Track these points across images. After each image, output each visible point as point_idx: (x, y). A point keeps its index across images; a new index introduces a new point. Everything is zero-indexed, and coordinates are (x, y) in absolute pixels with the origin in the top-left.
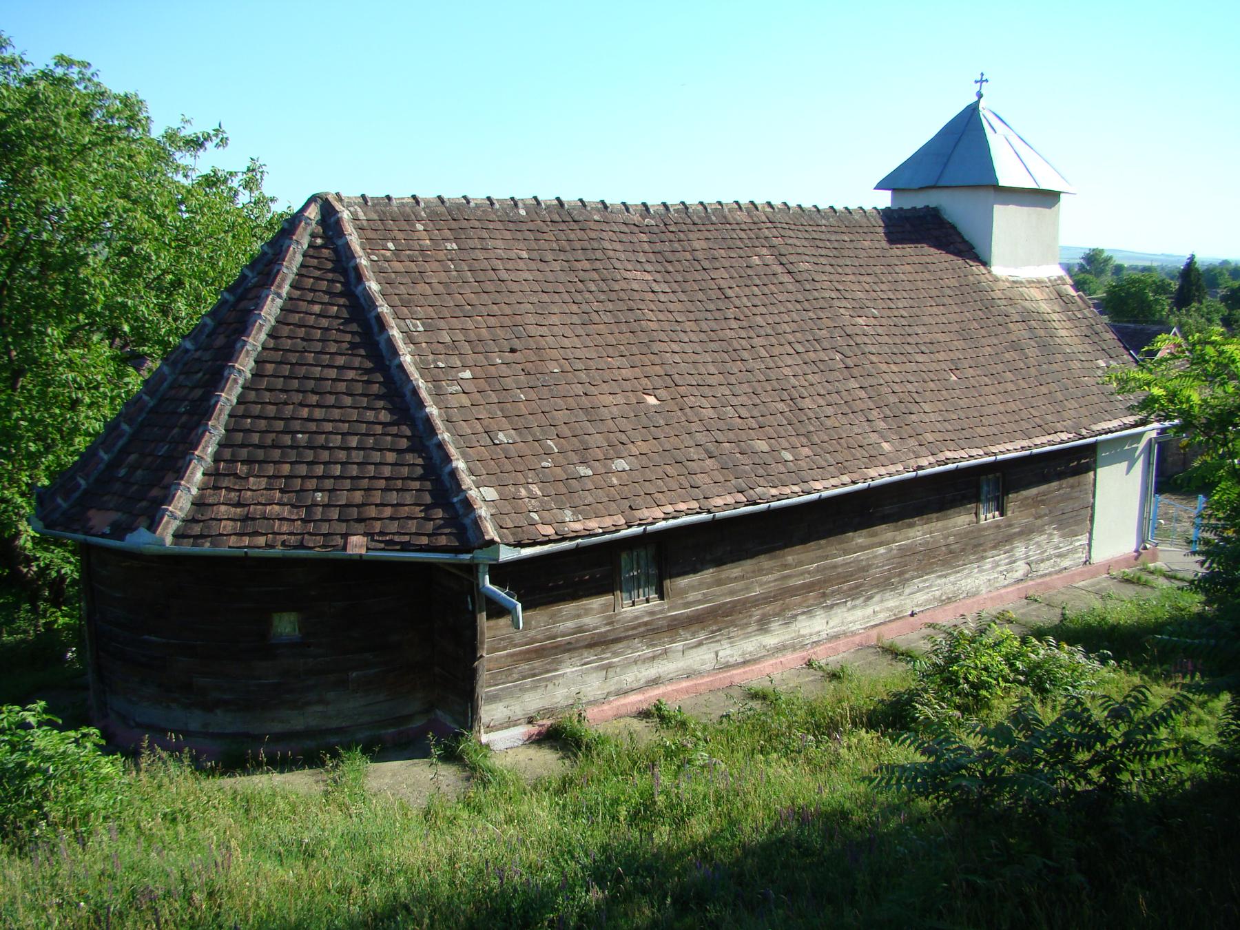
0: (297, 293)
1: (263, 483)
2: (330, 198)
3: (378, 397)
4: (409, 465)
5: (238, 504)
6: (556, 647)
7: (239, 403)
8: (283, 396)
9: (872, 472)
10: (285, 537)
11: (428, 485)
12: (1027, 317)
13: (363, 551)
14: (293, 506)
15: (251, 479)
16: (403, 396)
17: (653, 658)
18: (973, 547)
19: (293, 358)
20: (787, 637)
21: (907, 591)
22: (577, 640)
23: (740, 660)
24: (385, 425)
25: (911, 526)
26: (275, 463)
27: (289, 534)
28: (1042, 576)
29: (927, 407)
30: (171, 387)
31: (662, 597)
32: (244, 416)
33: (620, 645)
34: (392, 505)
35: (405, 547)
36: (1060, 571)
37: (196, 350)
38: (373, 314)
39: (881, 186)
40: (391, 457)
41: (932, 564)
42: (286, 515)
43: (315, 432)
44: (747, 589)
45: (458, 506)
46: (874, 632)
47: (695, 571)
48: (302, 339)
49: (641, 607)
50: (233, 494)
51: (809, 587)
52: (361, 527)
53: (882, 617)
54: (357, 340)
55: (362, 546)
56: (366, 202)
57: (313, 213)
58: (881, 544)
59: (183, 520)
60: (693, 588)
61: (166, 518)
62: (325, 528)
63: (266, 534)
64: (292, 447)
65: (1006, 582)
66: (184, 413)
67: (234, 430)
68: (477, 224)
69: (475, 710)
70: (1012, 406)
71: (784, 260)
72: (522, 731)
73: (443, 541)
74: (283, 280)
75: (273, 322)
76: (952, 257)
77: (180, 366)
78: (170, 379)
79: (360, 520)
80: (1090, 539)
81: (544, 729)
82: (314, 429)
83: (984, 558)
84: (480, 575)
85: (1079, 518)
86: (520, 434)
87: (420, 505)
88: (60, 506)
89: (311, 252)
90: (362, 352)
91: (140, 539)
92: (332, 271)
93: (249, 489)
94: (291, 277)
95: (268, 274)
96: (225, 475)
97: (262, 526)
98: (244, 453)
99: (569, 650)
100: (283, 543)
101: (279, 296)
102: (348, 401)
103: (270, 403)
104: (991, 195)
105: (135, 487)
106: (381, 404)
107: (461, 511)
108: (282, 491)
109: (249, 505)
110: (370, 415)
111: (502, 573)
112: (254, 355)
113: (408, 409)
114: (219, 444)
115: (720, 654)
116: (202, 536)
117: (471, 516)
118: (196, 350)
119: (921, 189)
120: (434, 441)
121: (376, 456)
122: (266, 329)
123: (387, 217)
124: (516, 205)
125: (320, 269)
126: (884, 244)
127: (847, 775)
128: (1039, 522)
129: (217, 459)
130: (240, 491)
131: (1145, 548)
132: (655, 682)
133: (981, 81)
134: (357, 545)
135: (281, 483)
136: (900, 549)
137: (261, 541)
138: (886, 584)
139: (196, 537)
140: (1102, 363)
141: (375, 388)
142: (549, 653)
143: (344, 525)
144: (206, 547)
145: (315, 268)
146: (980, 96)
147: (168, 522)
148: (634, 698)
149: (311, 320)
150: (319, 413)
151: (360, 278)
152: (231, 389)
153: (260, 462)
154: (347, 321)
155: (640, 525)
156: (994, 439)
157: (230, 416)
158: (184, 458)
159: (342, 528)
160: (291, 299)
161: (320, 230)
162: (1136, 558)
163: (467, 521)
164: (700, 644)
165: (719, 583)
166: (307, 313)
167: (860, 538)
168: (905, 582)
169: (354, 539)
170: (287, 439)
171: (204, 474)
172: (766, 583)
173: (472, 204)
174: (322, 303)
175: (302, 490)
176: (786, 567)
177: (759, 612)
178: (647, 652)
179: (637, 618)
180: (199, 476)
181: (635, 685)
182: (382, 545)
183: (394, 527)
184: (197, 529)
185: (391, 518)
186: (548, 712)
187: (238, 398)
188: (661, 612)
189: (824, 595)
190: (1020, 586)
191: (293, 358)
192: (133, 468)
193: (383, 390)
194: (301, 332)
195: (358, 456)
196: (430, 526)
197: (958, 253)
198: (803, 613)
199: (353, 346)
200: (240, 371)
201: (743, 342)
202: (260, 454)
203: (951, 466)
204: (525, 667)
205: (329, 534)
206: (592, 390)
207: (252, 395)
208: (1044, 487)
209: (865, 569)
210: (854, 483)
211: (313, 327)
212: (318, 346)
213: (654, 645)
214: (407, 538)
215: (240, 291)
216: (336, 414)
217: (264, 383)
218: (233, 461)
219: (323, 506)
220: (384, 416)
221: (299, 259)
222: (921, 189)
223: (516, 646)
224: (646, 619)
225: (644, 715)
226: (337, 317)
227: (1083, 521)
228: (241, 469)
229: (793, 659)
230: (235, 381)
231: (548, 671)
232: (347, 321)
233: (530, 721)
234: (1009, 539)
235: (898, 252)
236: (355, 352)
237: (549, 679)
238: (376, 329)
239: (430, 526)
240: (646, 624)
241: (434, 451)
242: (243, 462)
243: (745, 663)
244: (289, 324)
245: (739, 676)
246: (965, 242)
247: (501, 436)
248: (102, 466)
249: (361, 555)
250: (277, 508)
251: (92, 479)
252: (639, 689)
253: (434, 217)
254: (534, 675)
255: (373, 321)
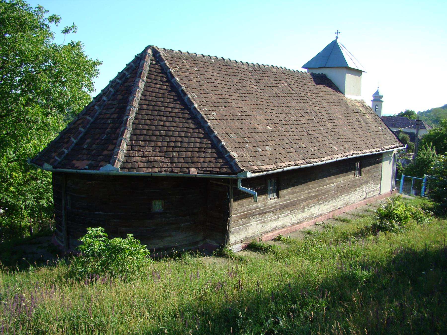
0: (149, 80)
1: (151, 149)
2: (155, 47)
3: (188, 119)
4: (205, 143)
5: (144, 156)
6: (250, 214)
7: (135, 119)
8: (152, 117)
9: (336, 156)
10: (165, 169)
11: (214, 150)
12: (358, 111)
13: (197, 174)
14: (165, 157)
15: (146, 147)
16: (198, 119)
17: (275, 220)
18: (353, 186)
19: (153, 103)
20: (309, 214)
21: (338, 200)
22: (256, 212)
23: (297, 222)
24: (193, 129)
25: (339, 177)
26: (154, 141)
27: (166, 167)
28: (369, 198)
29: (342, 137)
30: (100, 114)
31: (278, 198)
32: (139, 124)
33: (267, 214)
34: (203, 157)
35: (211, 172)
36: (373, 197)
37: (108, 101)
38: (180, 89)
39: (304, 67)
40: (198, 140)
41: (344, 191)
42: (163, 160)
43: (168, 131)
44: (300, 196)
45: (227, 158)
46: (331, 214)
47: (287, 188)
48: (155, 97)
49: (273, 201)
50: (140, 153)
51: (315, 196)
52: (193, 165)
53: (332, 209)
54: (176, 98)
55: (195, 172)
56: (166, 51)
57: (150, 51)
58: (332, 183)
59: (123, 162)
60: (287, 195)
61: (117, 161)
62: (180, 165)
63: (157, 168)
64: (160, 136)
65: (361, 199)
66: (111, 123)
67: (136, 129)
68: (201, 63)
69: (228, 237)
70: (363, 139)
71: (290, 86)
72: (240, 246)
73: (225, 170)
74: (144, 75)
75: (143, 90)
76: (333, 90)
77: (102, 106)
78: (99, 111)
79: (193, 162)
80: (380, 186)
81: (246, 245)
82: (167, 129)
83: (356, 190)
84: (239, 183)
85: (378, 179)
86: (236, 135)
87: (213, 157)
88: (57, 160)
89: (152, 66)
90: (179, 103)
91: (106, 169)
92: (160, 73)
93: (146, 151)
94: (146, 75)
95: (136, 73)
96: (136, 146)
97: (155, 165)
98: (141, 137)
99: (253, 215)
100: (165, 171)
101: (143, 81)
102: (177, 120)
103: (148, 119)
104: (345, 70)
105: (94, 151)
106: (190, 121)
107: (229, 160)
108: (159, 152)
109: (148, 157)
110: (187, 125)
111: (248, 182)
112: (138, 101)
113: (201, 124)
114: (131, 134)
115: (293, 219)
116: (132, 168)
117: (234, 161)
118: (108, 101)
119: (319, 68)
120: (213, 135)
121: (193, 140)
122: (141, 92)
123: (177, 57)
124: (211, 58)
125: (156, 72)
126: (314, 84)
127: (319, 268)
128: (369, 179)
129: (131, 140)
130: (143, 151)
131: (393, 190)
132: (275, 229)
133: (338, 33)
134: (194, 172)
135: (158, 149)
136: (337, 185)
137: (156, 170)
138: (334, 197)
139: (129, 168)
140: (380, 128)
141: (187, 116)
142: (248, 216)
143: (187, 164)
144: (134, 172)
145: (155, 72)
146: (337, 38)
147: (117, 163)
148: (270, 234)
149: (157, 90)
150: (167, 124)
151: (172, 77)
152: (132, 114)
153: (148, 141)
154: (170, 91)
155: (280, 168)
156: (361, 148)
157: (133, 124)
158: (117, 139)
159: (186, 165)
160: (148, 82)
161: (153, 58)
162: (391, 193)
163: (232, 163)
164: (287, 215)
165: (293, 193)
166: (154, 87)
167: (327, 180)
168: (338, 197)
169: (192, 170)
170: (157, 133)
171: (127, 145)
172: (305, 194)
173: (198, 56)
174: (160, 84)
175: (167, 152)
176: (309, 189)
177: (302, 205)
178: (274, 218)
179: (272, 204)
180: (125, 145)
181: (270, 230)
182: (203, 172)
183: (205, 165)
184: (129, 165)
185: (204, 162)
186: (247, 239)
187: (135, 117)
188: (278, 202)
189: (318, 200)
190: (365, 200)
191: (153, 103)
192: (90, 145)
193: (190, 117)
194: (154, 94)
195: (186, 140)
196: (219, 165)
197: (335, 89)
198: (313, 206)
199: (175, 100)
200: (134, 107)
201: (288, 111)
202: (148, 138)
203: (355, 156)
204: (241, 221)
205: (182, 168)
206: (252, 122)
207: (140, 116)
208: (370, 167)
209: (328, 191)
210: (332, 159)
211: (158, 93)
212: (162, 100)
213: (276, 215)
214: (211, 169)
215: (123, 79)
216: (174, 124)
217: (144, 112)
218: (138, 140)
219: (177, 157)
220: (192, 126)
221: (148, 68)
222: (319, 68)
223: (239, 213)
224: (274, 205)
225: (274, 240)
226: (166, 90)
227: (379, 179)
228: (142, 144)
229: (311, 222)
230: (133, 111)
231: (247, 223)
232: (170, 91)
233: (242, 242)
234: (362, 184)
235: (319, 87)
236: (176, 102)
237: (247, 226)
238: (182, 95)
239: (219, 165)
240: (274, 207)
241: (214, 139)
242: (142, 141)
243: (298, 223)
244: (149, 91)
245: (299, 227)
246: (335, 86)
247: (231, 135)
248: (73, 145)
249: (196, 175)
250: (159, 158)
251: (70, 150)
252: (270, 231)
253: (187, 59)
254: (243, 225)
255: (181, 92)
